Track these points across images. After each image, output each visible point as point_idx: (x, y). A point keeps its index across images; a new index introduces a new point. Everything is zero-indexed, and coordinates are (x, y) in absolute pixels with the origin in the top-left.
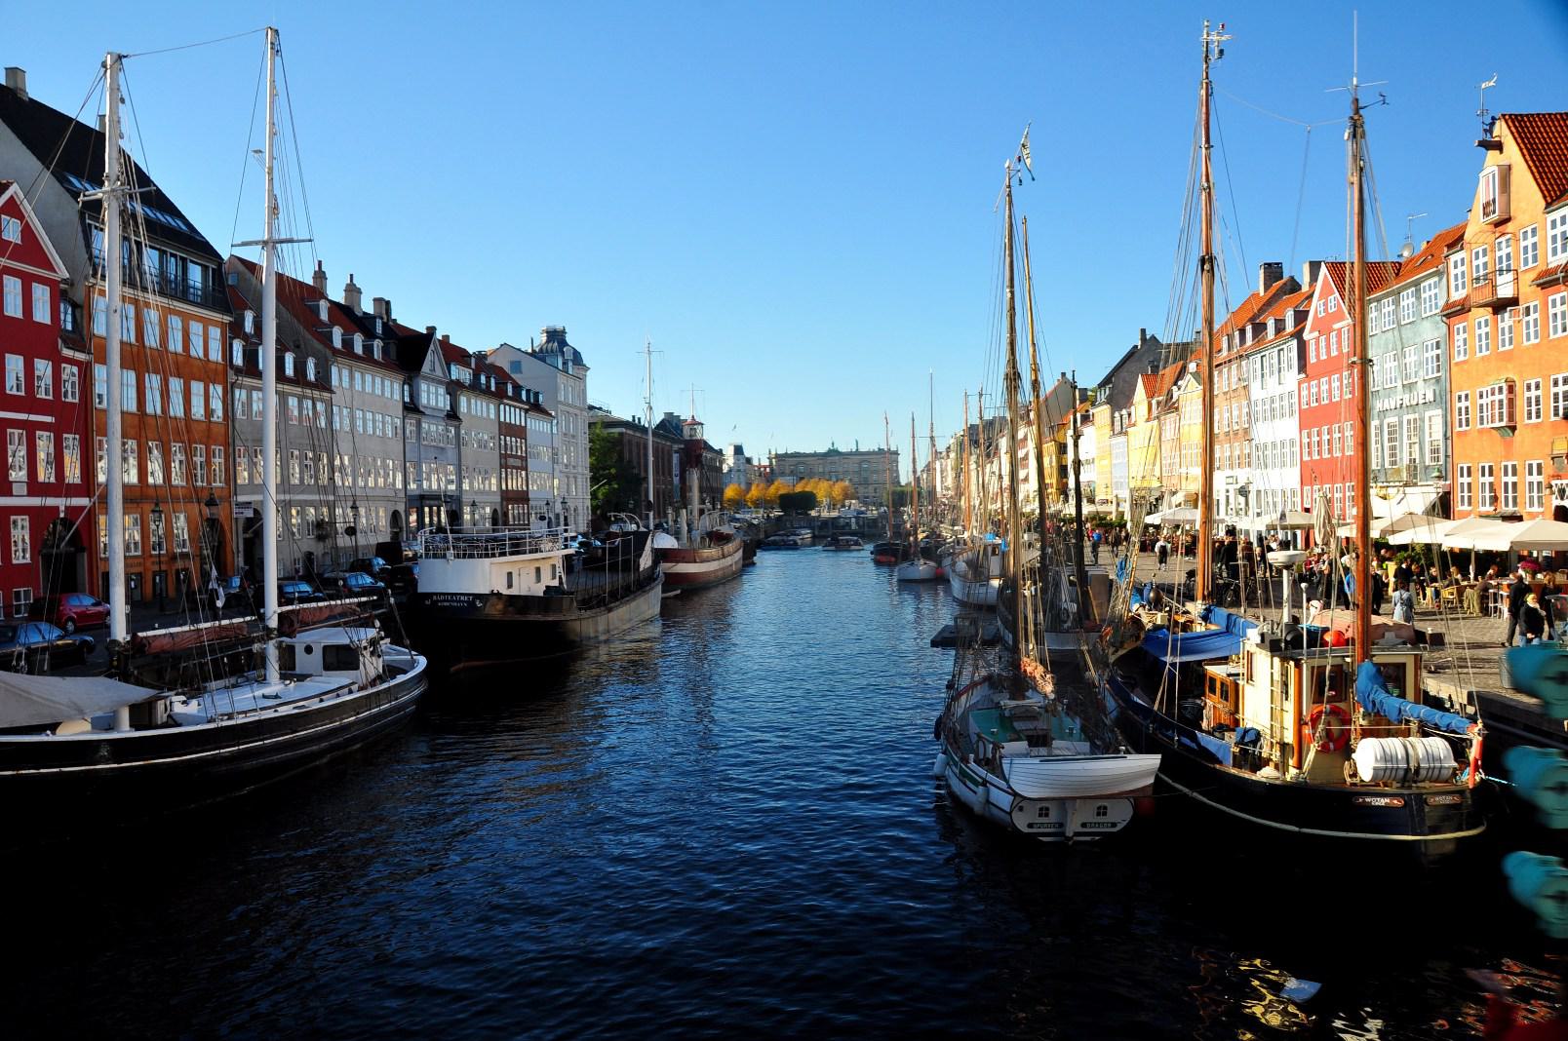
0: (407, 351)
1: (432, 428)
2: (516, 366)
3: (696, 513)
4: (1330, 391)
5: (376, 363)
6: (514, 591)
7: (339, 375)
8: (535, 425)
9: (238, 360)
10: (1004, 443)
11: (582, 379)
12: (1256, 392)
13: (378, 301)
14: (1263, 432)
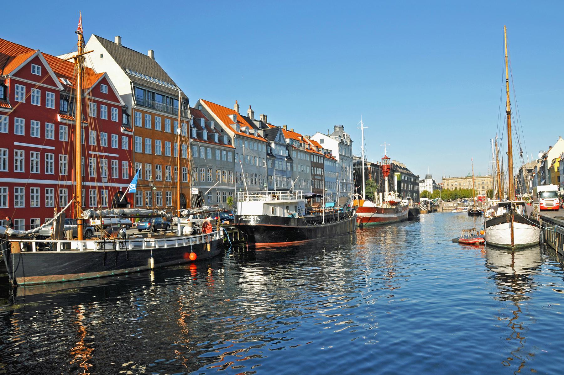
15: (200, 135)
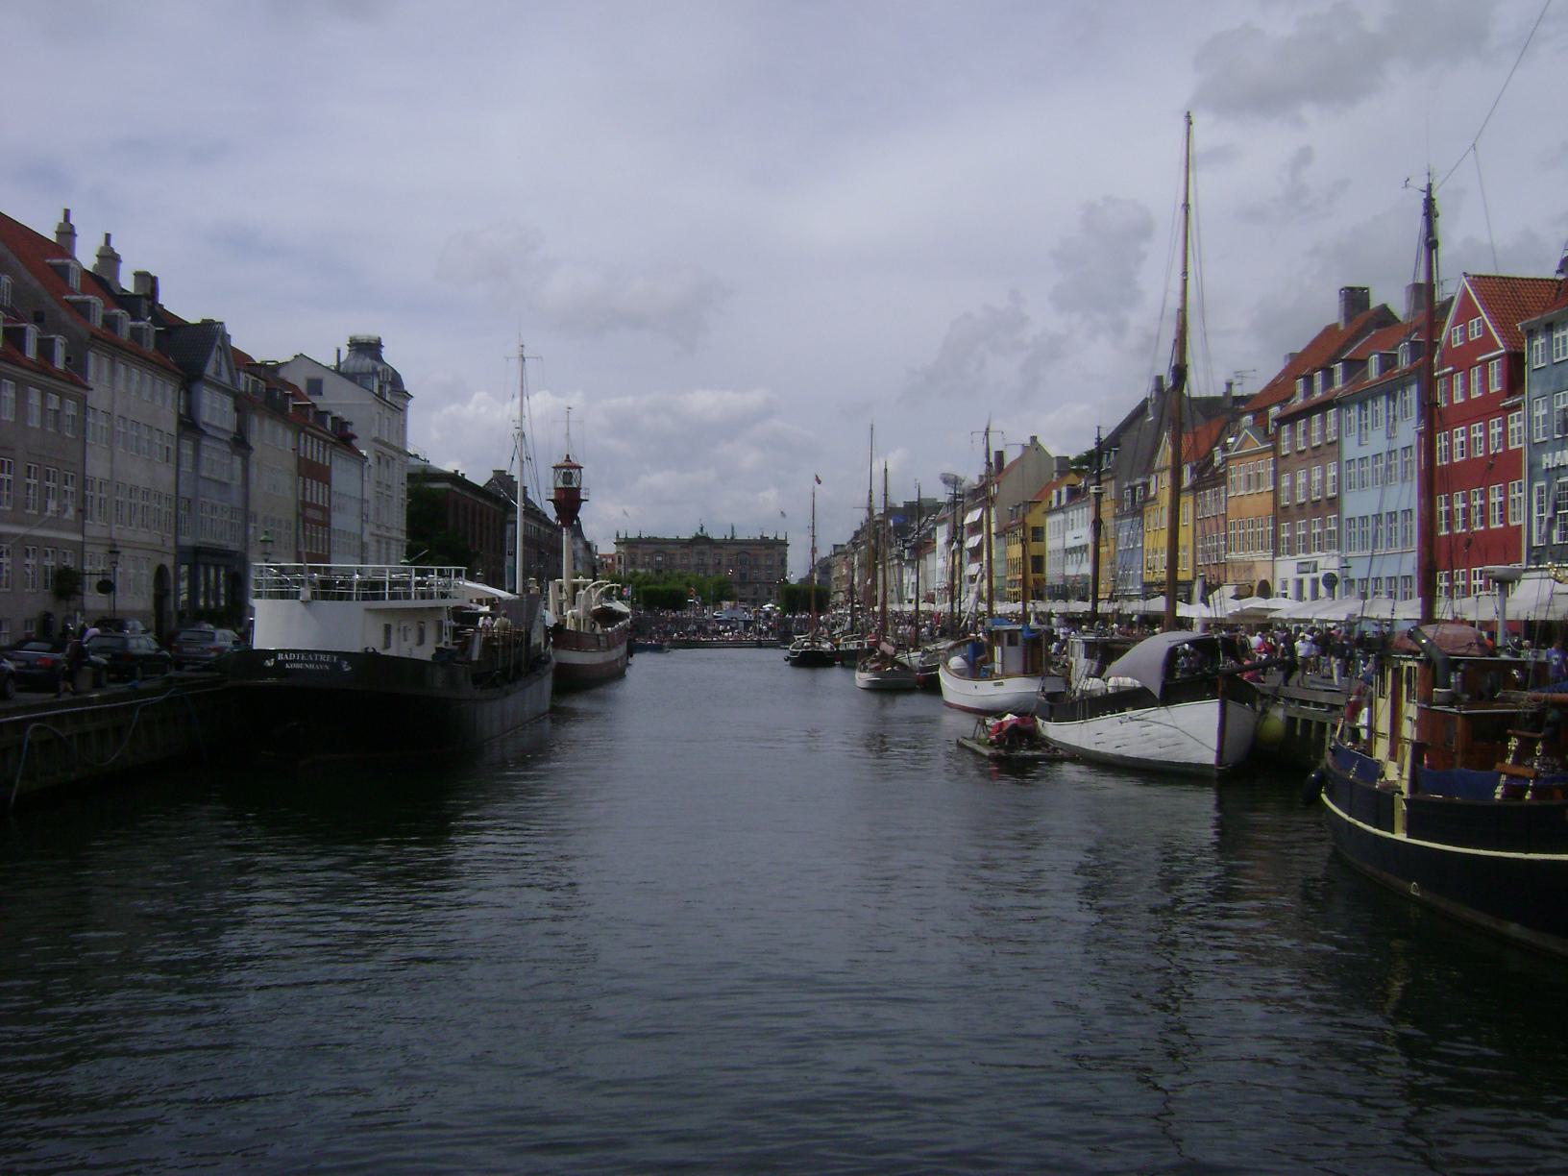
0: (188, 351)
1: (217, 461)
2: (315, 386)
4: (1323, 481)
6: (392, 652)
7: (97, 367)
10: (942, 536)
11: (400, 410)
12: (1350, 448)
14: (1358, 504)
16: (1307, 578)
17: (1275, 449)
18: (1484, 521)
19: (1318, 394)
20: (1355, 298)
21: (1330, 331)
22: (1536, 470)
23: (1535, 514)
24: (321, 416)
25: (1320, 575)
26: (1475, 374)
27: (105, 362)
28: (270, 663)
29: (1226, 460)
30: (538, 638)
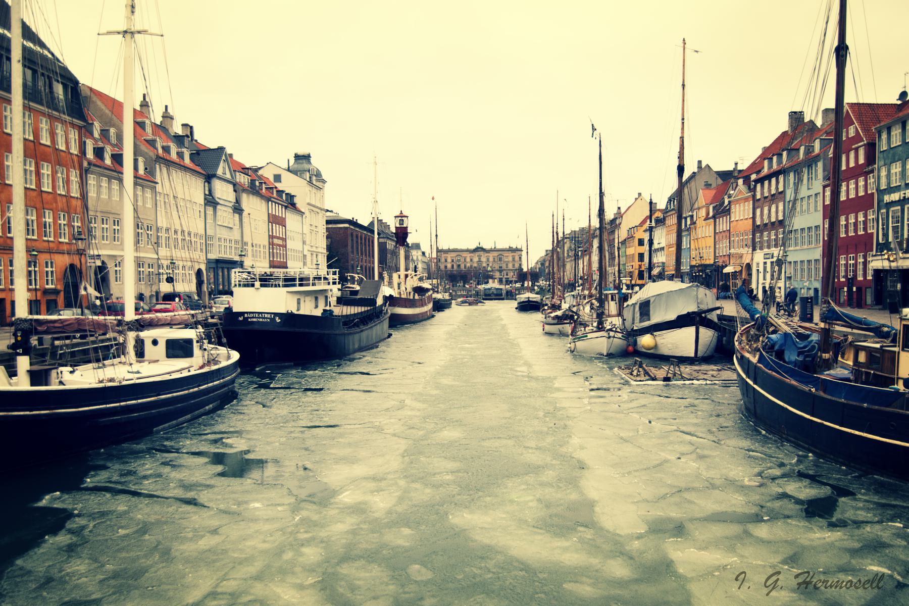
0: (206, 162)
1: (225, 214)
2: (278, 178)
3: (402, 277)
5: (185, 168)
6: (301, 312)
8: (291, 219)
9: (90, 155)
13: (185, 125)
15: (99, 153)
16: (769, 261)
17: (754, 196)
18: (856, 230)
19: (775, 166)
20: (796, 118)
21: (784, 134)
22: (881, 204)
23: (880, 227)
24: (280, 192)
25: (775, 259)
26: (852, 155)
27: (164, 170)
28: (241, 319)
29: (730, 202)
30: (380, 301)
